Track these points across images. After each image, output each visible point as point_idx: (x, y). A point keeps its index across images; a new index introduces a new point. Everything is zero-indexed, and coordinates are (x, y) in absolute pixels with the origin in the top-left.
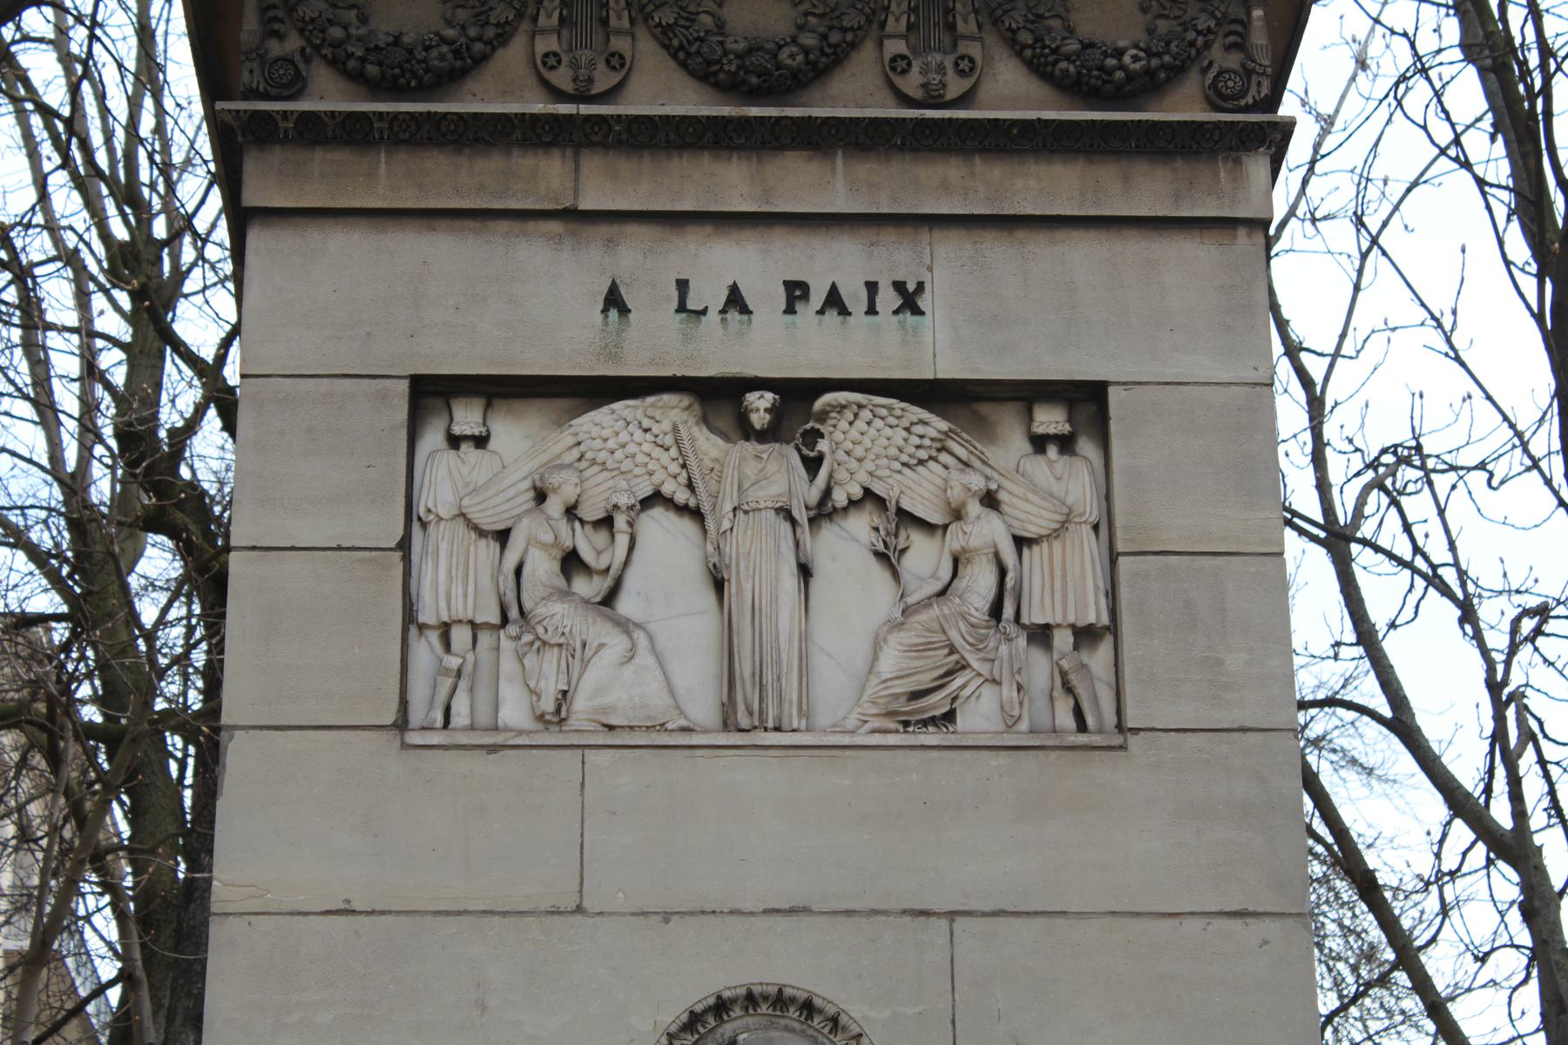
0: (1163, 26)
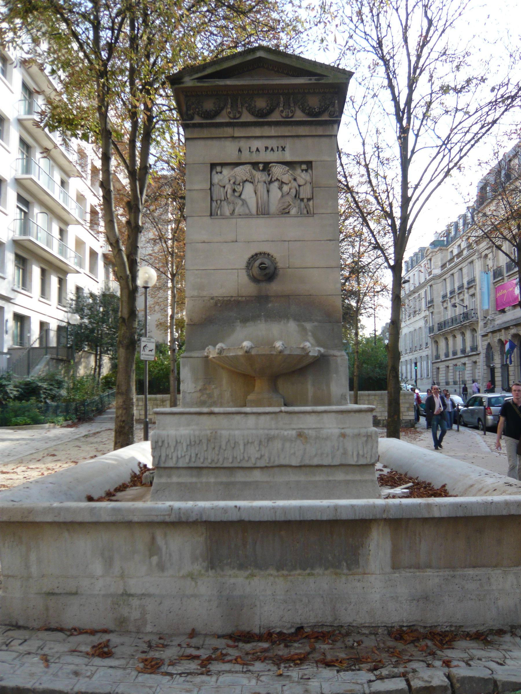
0: (323, 104)
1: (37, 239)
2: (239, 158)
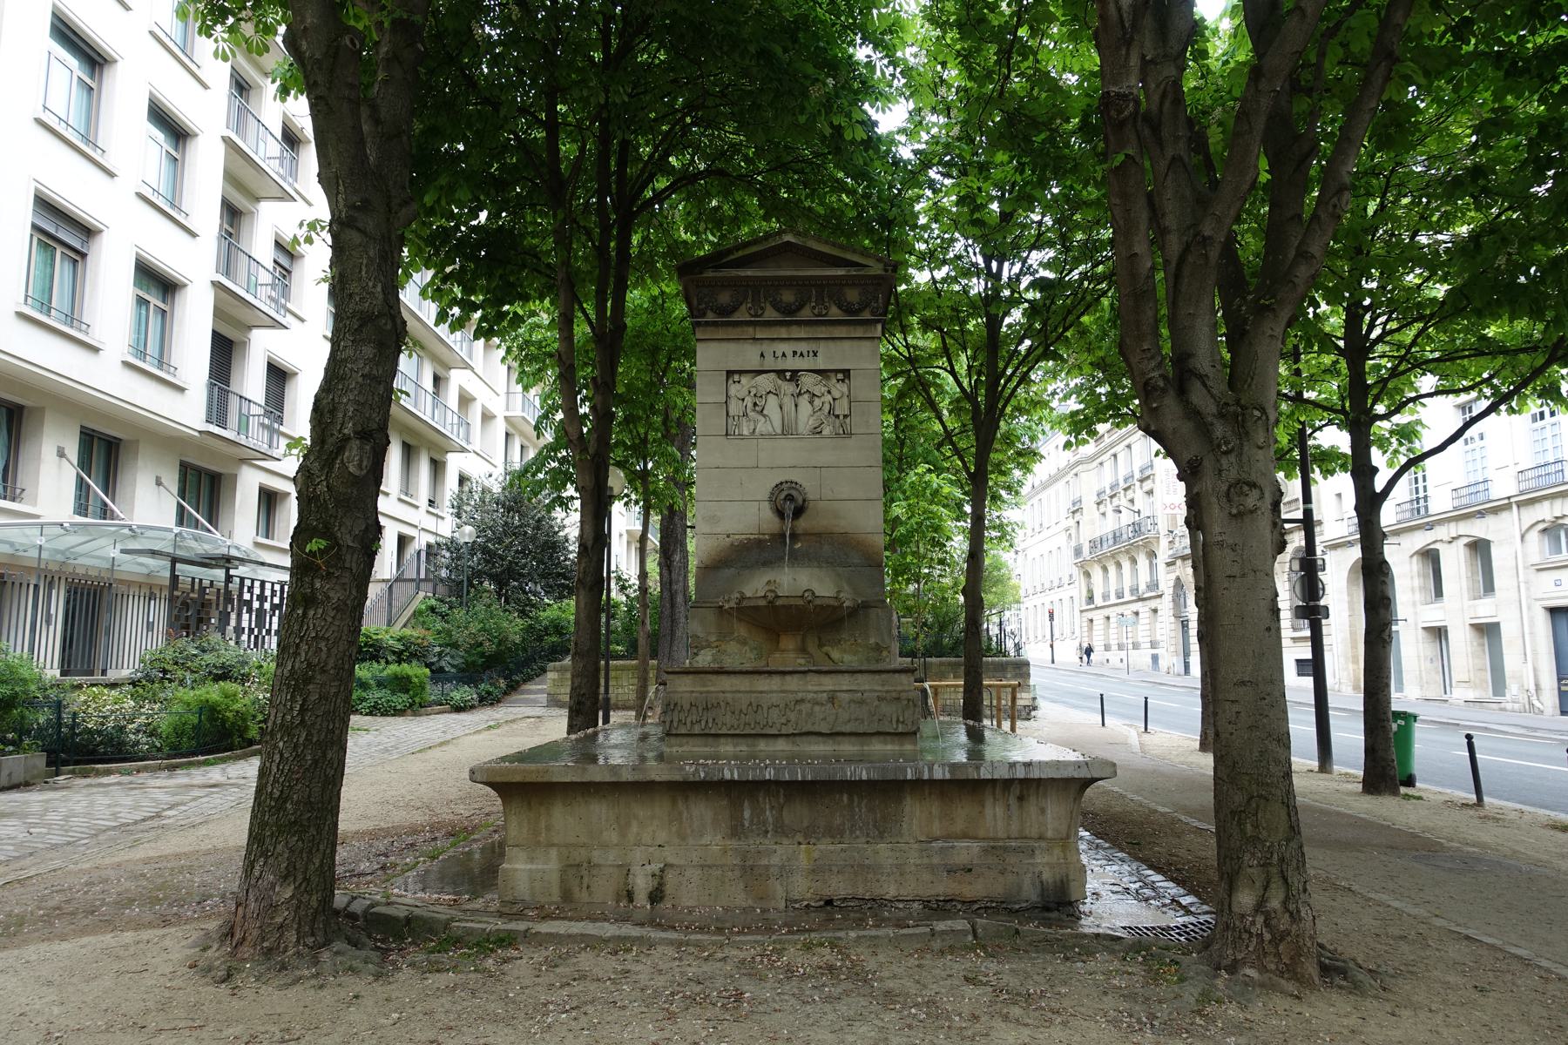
1: (433, 419)
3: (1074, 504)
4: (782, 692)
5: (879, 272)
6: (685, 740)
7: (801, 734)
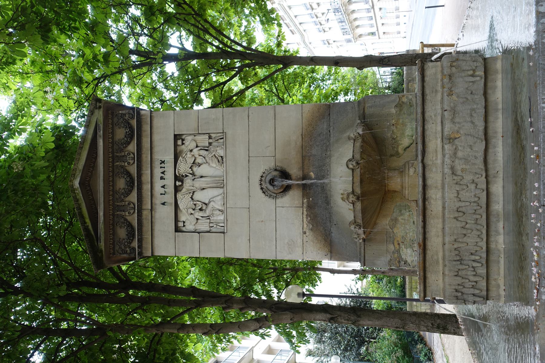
0: (122, 126)
2: (171, 204)
3: (325, 44)
4: (443, 188)
5: (101, 112)
6: (493, 283)
7: (486, 170)
